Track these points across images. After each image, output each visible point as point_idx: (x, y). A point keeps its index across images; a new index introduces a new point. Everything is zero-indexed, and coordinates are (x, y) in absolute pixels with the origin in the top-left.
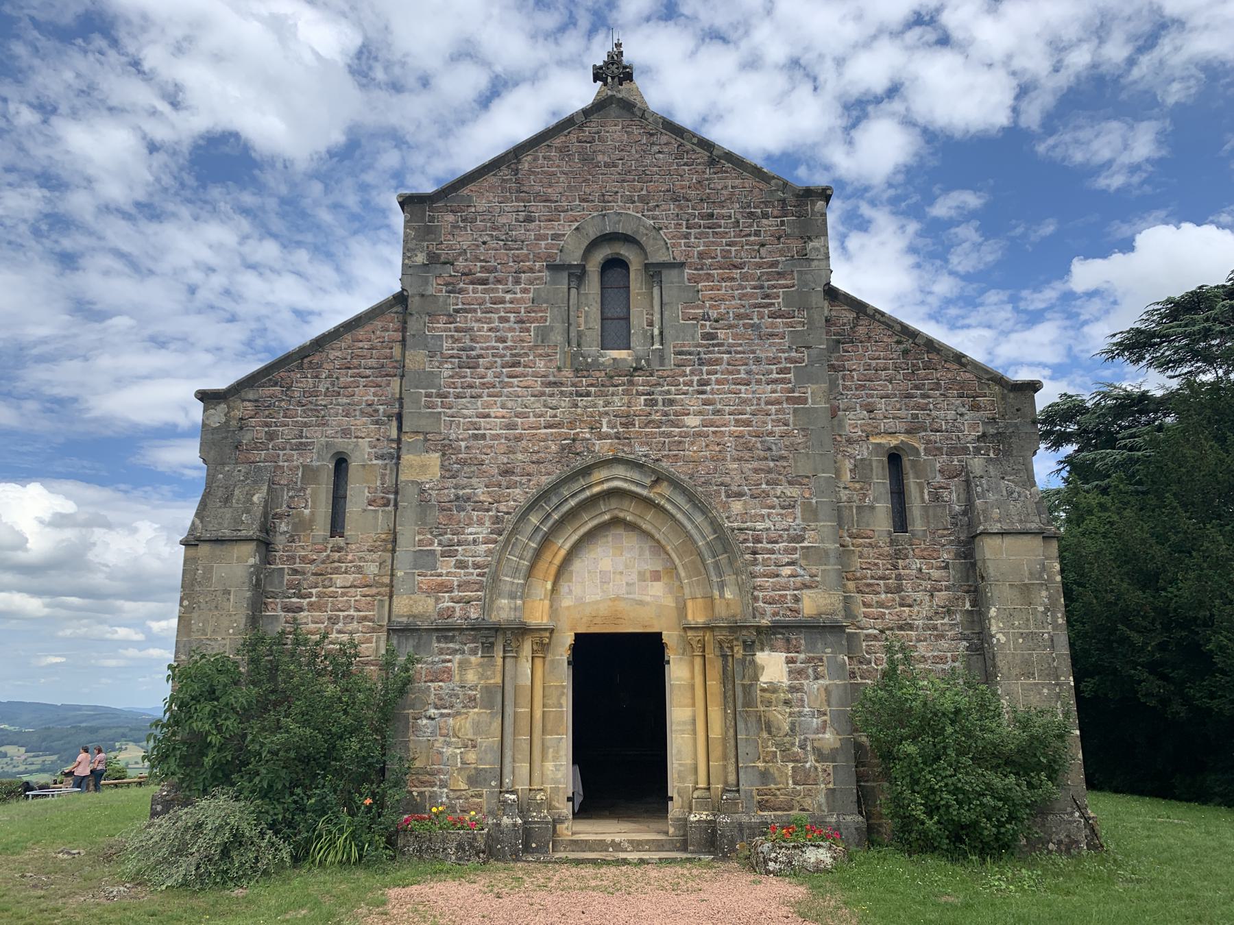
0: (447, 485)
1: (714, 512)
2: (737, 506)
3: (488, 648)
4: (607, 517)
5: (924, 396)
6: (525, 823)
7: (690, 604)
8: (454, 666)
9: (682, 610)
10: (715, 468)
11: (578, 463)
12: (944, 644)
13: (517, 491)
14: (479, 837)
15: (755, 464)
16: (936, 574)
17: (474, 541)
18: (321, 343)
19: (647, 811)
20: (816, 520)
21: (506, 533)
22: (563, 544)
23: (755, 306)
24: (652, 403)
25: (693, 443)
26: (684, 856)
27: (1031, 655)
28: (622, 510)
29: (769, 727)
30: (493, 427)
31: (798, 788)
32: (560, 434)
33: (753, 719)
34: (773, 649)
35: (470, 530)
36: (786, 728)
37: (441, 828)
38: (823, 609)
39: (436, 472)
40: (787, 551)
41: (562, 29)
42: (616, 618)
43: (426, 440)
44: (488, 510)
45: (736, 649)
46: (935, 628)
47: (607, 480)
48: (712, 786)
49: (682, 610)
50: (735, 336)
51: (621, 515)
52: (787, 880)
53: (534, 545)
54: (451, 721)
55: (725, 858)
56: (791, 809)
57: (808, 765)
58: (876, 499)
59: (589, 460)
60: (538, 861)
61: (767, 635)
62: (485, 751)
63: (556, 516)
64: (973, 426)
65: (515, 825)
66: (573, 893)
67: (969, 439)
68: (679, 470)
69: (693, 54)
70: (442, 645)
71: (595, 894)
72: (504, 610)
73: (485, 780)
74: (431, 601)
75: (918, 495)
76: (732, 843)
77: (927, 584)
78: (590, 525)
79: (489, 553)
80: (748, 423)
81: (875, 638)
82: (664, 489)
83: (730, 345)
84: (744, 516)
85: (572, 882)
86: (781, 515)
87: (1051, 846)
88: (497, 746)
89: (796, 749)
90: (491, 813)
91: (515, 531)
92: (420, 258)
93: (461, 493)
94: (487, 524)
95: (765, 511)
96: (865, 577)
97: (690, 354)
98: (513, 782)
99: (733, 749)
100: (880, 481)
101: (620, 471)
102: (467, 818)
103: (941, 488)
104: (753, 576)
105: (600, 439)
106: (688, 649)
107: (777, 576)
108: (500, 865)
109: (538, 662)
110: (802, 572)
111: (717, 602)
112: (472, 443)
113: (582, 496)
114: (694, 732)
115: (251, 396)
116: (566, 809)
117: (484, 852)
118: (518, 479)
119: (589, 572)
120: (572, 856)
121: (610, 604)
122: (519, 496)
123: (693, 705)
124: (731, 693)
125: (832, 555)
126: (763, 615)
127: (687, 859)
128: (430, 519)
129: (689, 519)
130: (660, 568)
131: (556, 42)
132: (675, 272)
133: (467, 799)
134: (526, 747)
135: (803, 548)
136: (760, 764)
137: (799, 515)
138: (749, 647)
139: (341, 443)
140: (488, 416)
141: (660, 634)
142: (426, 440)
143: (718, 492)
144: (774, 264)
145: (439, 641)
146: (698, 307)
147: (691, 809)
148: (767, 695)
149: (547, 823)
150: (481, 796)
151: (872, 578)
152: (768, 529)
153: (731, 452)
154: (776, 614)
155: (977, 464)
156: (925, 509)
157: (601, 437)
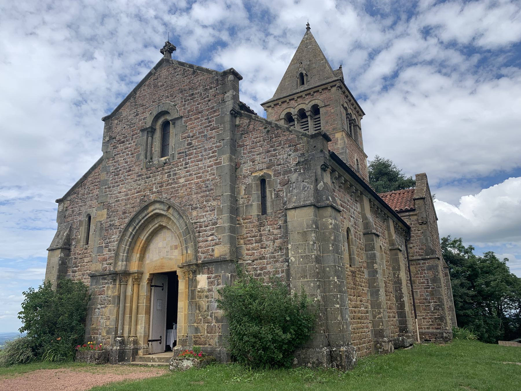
2: (195, 213)
5: (275, 150)
10: (188, 199)
12: (278, 265)
15: (202, 194)
16: (276, 232)
18: (86, 176)
20: (222, 214)
23: (206, 127)
24: (169, 176)
25: (181, 189)
27: (306, 266)
30: (122, 197)
31: (209, 335)
33: (194, 305)
34: (203, 274)
36: (205, 308)
38: (222, 253)
39: (105, 216)
41: (395, 23)
43: (104, 205)
44: (118, 228)
46: (275, 257)
50: (198, 142)
54: (104, 309)
56: (205, 344)
57: (212, 325)
58: (253, 201)
64: (294, 159)
67: (292, 166)
69: (462, 10)
72: (120, 266)
74: (101, 265)
75: (270, 196)
77: (272, 237)
80: (200, 177)
81: (250, 264)
83: (197, 146)
84: (197, 217)
87: (309, 365)
92: (107, 139)
93: (111, 223)
96: (247, 237)
97: (183, 153)
100: (256, 193)
103: (279, 191)
107: (207, 241)
110: (215, 238)
112: (116, 203)
115: (69, 199)
125: (227, 228)
128: (102, 234)
131: (394, 30)
132: (179, 121)
135: (216, 227)
137: (216, 213)
138: (195, 273)
139: (89, 211)
140: (120, 192)
141: (175, 272)
142: (104, 205)
143: (188, 208)
144: (213, 108)
146: (186, 133)
148: (200, 294)
150: (109, 338)
151: (250, 237)
152: (205, 221)
154: (205, 258)
155: (294, 177)
156: (272, 202)
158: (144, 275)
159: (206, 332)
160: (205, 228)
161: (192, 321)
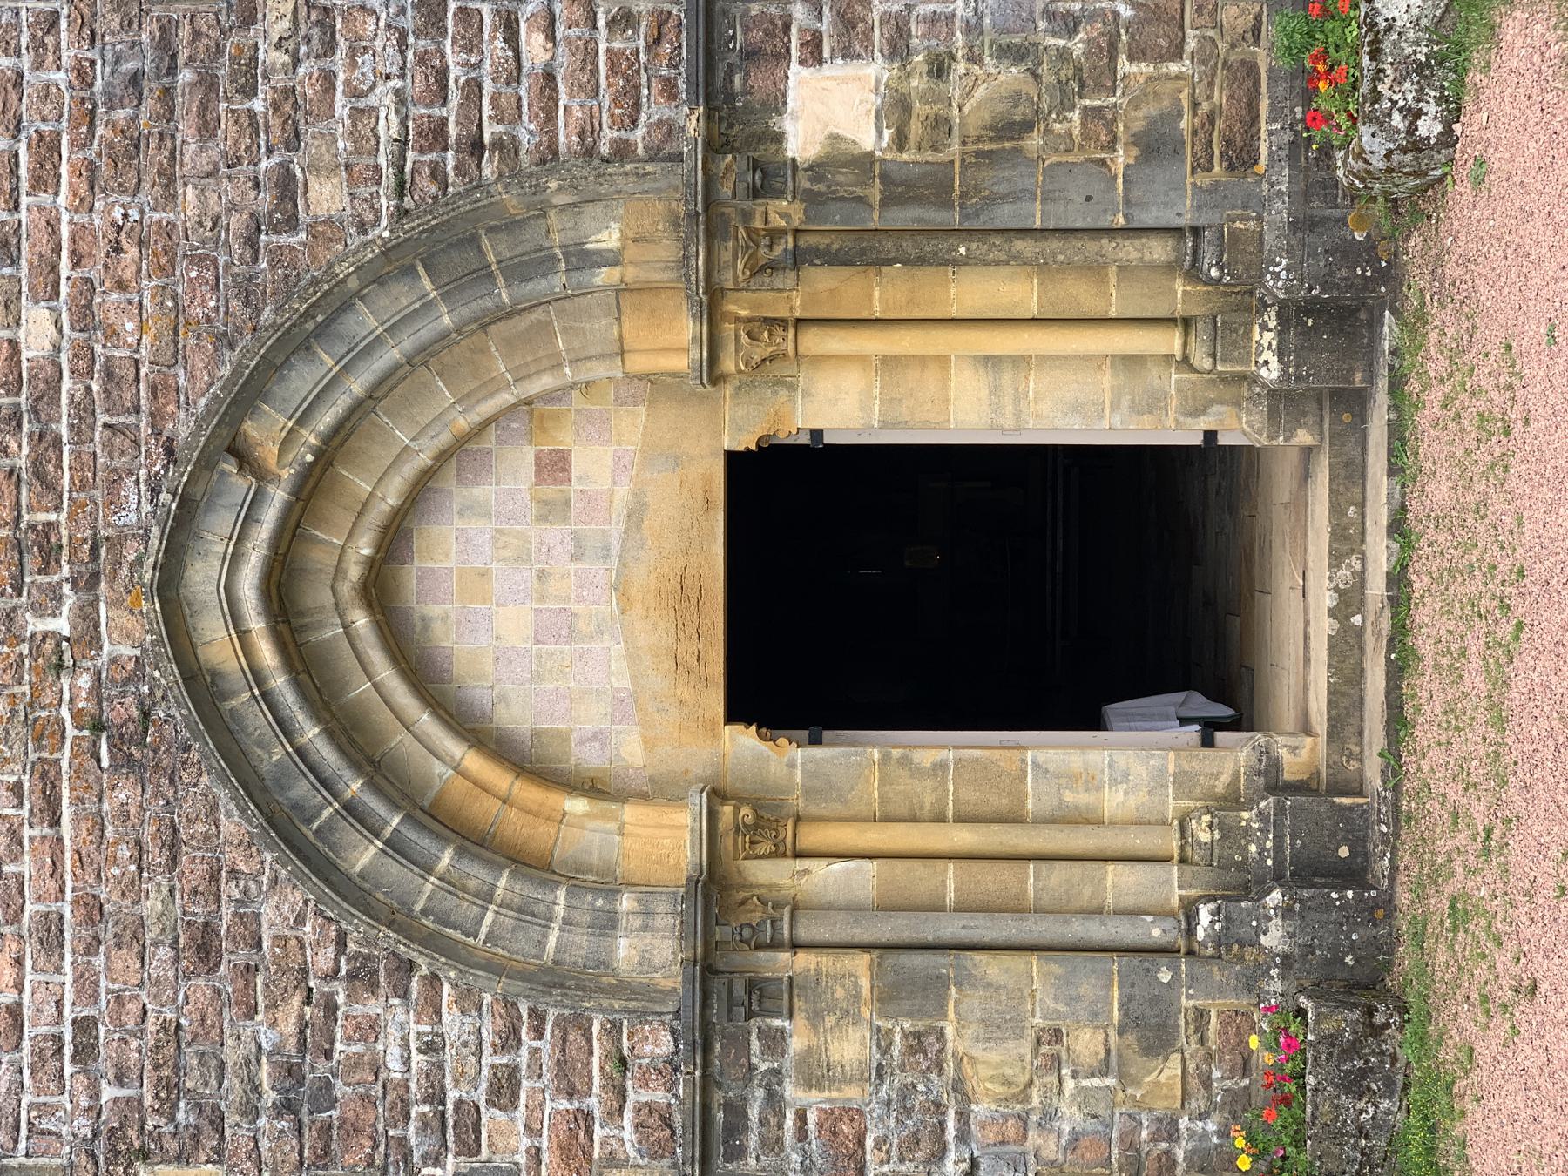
0: (245, 1142)
1: (342, 271)
2: (325, 196)
3: (763, 996)
4: (361, 620)
6: (1278, 878)
7: (639, 363)
8: (815, 1101)
9: (656, 385)
10: (198, 261)
11: (176, 712)
13: (268, 912)
14: (1329, 1027)
15: (186, 129)
17: (430, 1048)
19: (1232, 509)
21: (404, 945)
22: (444, 761)
25: (112, 334)
26: (1382, 398)
28: (339, 572)
29: (1010, 129)
31: (1191, 44)
32: (78, 773)
33: (993, 179)
34: (777, 104)
35: (394, 1063)
36: (1012, 75)
37: (1298, 1142)
40: (471, 44)
42: (683, 593)
44: (331, 1008)
45: (778, 222)
47: (235, 617)
48: (1180, 310)
49: (656, 385)
51: (354, 572)
52: (1473, 77)
53: (447, 857)
54: (981, 1109)
55: (1392, 275)
56: (1251, 69)
59: (166, 675)
60: (1391, 842)
61: (736, 125)
62: (1071, 1000)
63: (354, 786)
65: (1287, 912)
66: (1515, 750)
68: (203, 379)
70: (753, 1140)
71: (1519, 682)
72: (649, 949)
73: (1155, 1001)
76: (1348, 252)
78: (386, 673)
79: (468, 1000)
80: (47, 148)
82: (265, 431)
84: (357, 174)
85: (1474, 741)
86: (353, 53)
88: (1056, 966)
89: (1077, 46)
90: (1251, 982)
91: (398, 919)
93: (270, 1096)
94: (374, 1007)
95: (342, 105)
98: (1161, 913)
99: (1076, 243)
101: (203, 576)
102: (1268, 1059)
104: (549, 156)
105: (95, 641)
106: (777, 371)
107: (549, 77)
108: (1405, 956)
109: (812, 837)
111: (631, 273)
112: (105, 1065)
113: (288, 697)
114: (1020, 361)
116: (1236, 755)
117: (1370, 1012)
118: (227, 912)
119: (537, 677)
120: (1375, 736)
121: (637, 611)
122: (283, 907)
123: (942, 360)
124: (907, 245)
126: (671, 130)
127: (1395, 387)
129: (368, 351)
130: (528, 454)
133: (1209, 1057)
134: (1059, 874)
136: (1121, 159)
138: (769, 176)
141: (732, 458)
143: (277, 254)
145: (742, 1152)
147: (1243, 377)
148: (915, 129)
149: (1280, 810)
150: (1201, 1016)
153: (142, 208)
157: (88, 635)
158: (729, 783)
159: (1174, 68)
160: (455, 97)
161: (1096, 189)
